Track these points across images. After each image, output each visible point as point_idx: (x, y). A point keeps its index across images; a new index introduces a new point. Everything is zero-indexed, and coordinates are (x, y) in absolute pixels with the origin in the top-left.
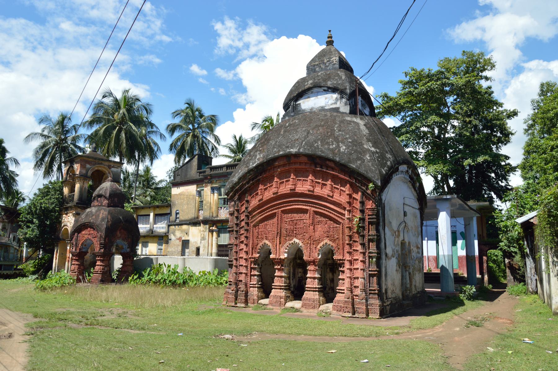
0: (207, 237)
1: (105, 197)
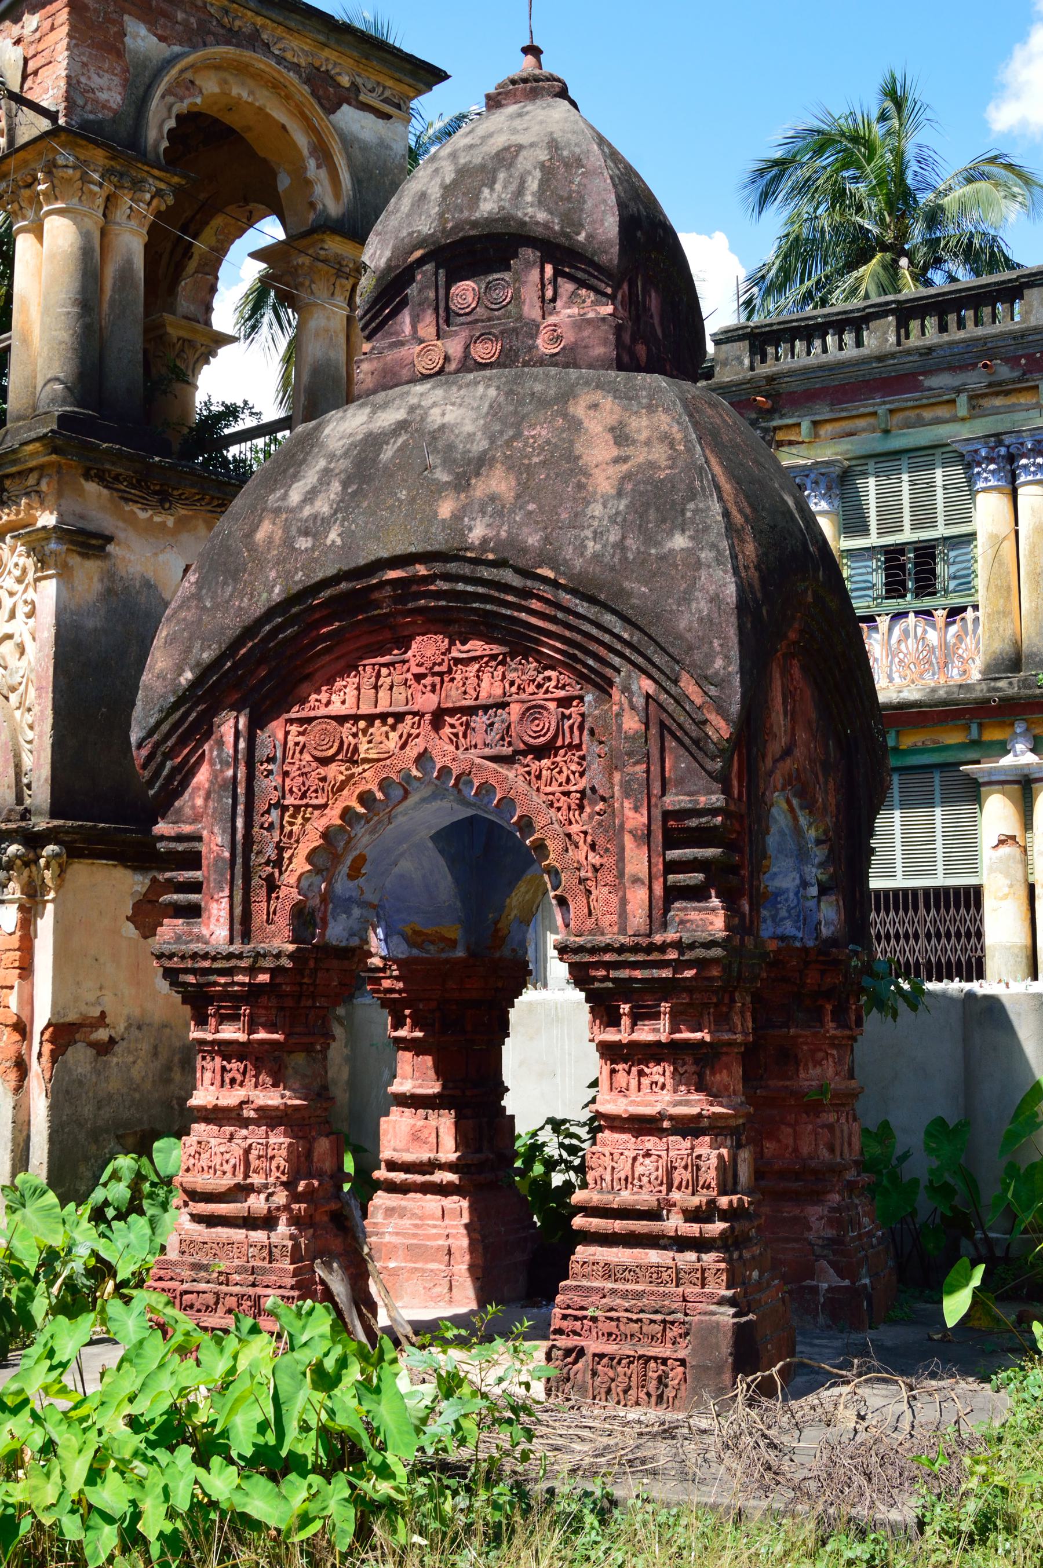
1: (566, 257)
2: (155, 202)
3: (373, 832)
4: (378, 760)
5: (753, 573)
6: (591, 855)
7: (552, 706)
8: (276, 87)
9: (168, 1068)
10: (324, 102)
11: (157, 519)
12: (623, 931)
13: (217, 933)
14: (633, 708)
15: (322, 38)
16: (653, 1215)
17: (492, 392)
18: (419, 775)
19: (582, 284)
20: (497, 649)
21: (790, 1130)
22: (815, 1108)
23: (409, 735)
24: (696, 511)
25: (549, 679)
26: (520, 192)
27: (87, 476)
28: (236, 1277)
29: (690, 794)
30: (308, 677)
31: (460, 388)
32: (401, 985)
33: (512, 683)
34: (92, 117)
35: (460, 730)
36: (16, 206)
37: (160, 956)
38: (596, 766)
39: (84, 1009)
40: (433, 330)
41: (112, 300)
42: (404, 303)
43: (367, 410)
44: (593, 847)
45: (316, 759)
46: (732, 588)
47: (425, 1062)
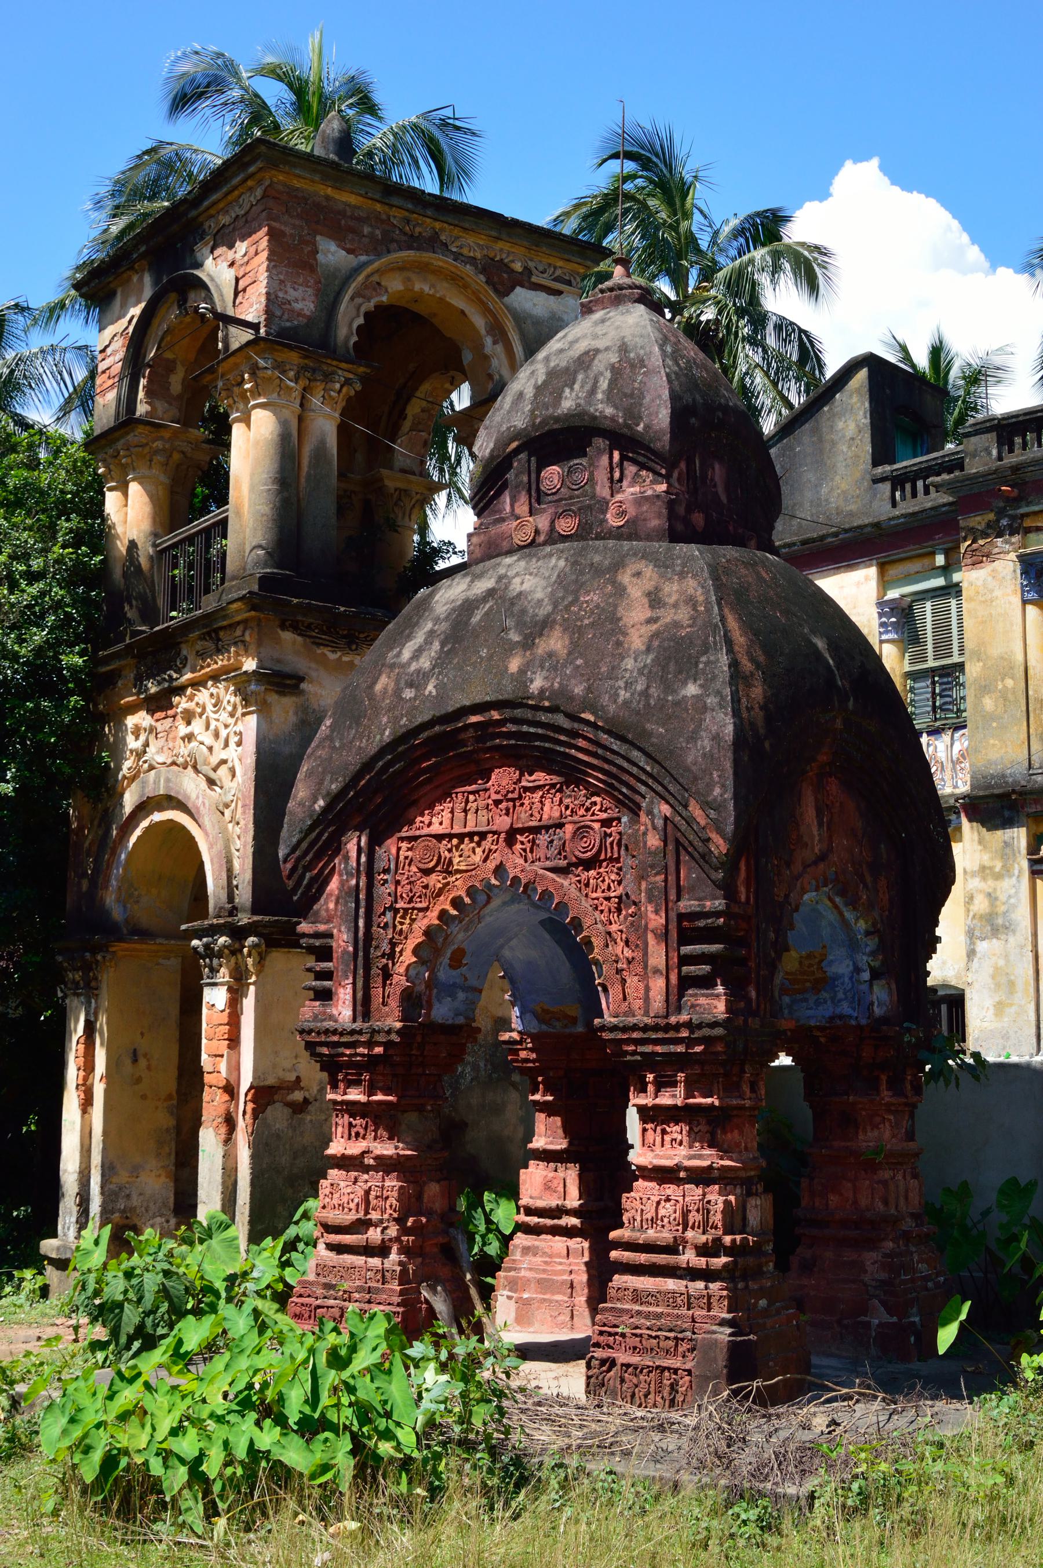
0: (1022, 914)
1: (629, 445)
2: (344, 390)
3: (466, 930)
4: (467, 871)
5: (759, 715)
6: (626, 950)
7: (596, 826)
8: (456, 280)
10: (499, 287)
11: (345, 659)
12: (646, 1013)
14: (654, 828)
15: (494, 234)
16: (672, 1249)
17: (562, 563)
18: (497, 883)
19: (642, 466)
20: (556, 779)
21: (849, 1185)
22: (871, 1166)
23: (490, 850)
24: (707, 663)
25: (595, 803)
26: (593, 391)
27: (283, 627)
28: (356, 1295)
29: (699, 900)
30: (414, 803)
31: (538, 560)
32: (534, 1056)
33: (567, 807)
34: (288, 324)
35: (528, 846)
36: (231, 400)
37: (302, 1032)
38: (629, 877)
39: (281, 1074)
40: (526, 508)
41: (309, 474)
42: (504, 486)
43: (468, 579)
44: (627, 943)
46: (730, 728)
47: (555, 1122)
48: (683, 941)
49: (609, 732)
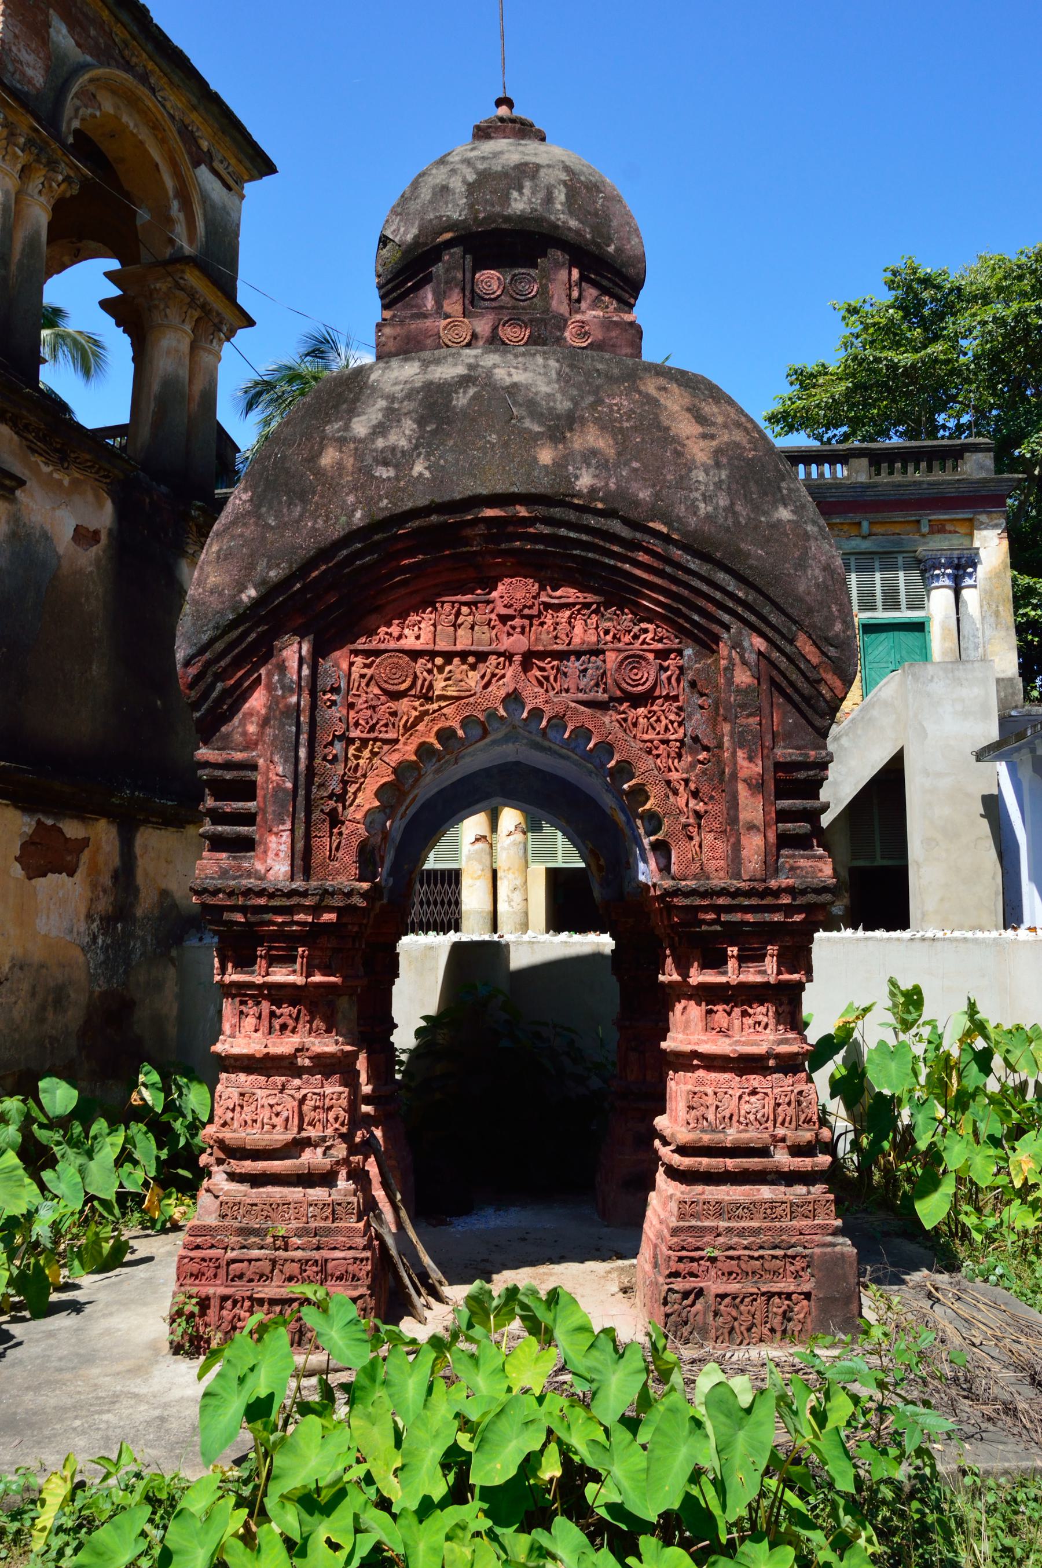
2: (63, 186)
4: (458, 698)
6: (692, 803)
7: (651, 656)
8: (155, 127)
9: (43, 1008)
11: (56, 476)
13: (276, 867)
14: (744, 663)
15: (194, 101)
19: (605, 291)
20: (590, 598)
25: (646, 631)
28: (297, 1241)
30: (377, 609)
33: (607, 632)
40: (459, 308)
42: (427, 280)
45: (385, 692)
48: (779, 796)
49: (686, 548)
